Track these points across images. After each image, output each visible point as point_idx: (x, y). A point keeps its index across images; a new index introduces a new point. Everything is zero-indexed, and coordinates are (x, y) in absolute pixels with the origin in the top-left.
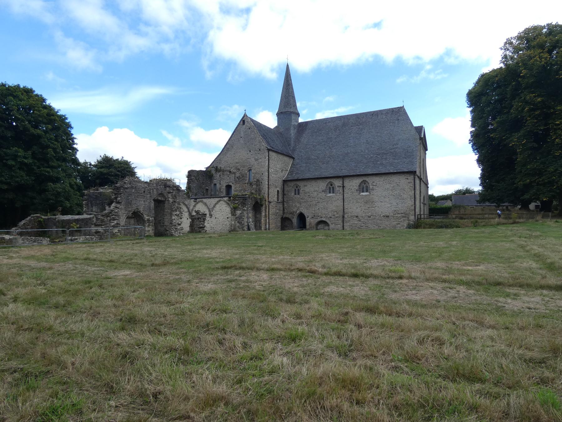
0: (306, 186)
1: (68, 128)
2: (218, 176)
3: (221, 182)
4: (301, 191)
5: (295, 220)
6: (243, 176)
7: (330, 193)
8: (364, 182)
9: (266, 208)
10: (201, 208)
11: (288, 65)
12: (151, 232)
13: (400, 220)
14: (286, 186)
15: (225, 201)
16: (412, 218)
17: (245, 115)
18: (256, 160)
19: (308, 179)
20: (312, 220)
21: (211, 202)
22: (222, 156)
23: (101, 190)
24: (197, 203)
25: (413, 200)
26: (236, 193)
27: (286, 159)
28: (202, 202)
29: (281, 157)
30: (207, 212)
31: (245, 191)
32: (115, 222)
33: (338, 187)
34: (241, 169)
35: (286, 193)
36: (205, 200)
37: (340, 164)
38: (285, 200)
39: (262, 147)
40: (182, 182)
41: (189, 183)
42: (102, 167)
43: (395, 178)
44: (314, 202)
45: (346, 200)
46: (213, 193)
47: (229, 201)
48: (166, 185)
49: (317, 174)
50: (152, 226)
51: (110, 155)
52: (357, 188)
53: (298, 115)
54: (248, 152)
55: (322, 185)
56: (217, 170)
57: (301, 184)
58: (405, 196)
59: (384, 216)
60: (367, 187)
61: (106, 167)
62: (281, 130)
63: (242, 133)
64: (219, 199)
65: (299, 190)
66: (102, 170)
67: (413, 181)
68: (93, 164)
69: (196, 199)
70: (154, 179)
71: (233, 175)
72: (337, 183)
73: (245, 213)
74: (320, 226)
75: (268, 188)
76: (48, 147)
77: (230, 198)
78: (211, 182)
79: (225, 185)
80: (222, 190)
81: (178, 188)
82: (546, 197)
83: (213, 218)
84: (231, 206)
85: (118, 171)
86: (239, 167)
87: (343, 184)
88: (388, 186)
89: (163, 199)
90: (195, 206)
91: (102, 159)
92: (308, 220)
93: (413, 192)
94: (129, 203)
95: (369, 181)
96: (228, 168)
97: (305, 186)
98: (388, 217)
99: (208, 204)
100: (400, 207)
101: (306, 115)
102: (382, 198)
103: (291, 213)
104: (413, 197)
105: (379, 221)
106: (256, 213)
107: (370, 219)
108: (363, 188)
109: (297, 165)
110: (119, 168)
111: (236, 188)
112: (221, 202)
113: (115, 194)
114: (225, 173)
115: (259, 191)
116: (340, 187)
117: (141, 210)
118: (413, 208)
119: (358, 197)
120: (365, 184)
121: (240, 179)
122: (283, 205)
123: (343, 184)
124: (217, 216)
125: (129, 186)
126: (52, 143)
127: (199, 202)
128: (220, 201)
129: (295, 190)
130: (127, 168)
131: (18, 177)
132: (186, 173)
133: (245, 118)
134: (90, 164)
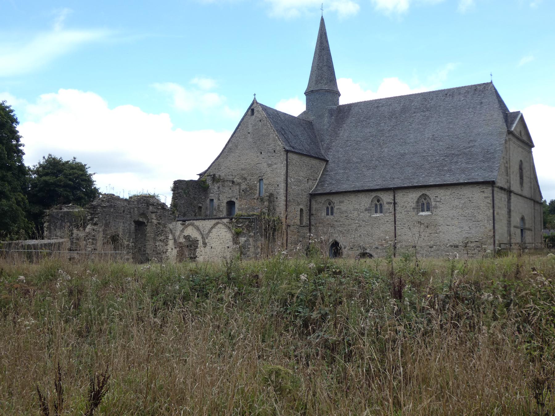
0: (342, 202)
1: (13, 123)
2: (216, 188)
3: (220, 197)
4: (335, 210)
6: (251, 189)
7: (376, 212)
8: (424, 196)
10: (190, 231)
11: (322, 20)
13: (473, 252)
14: (313, 202)
15: (225, 224)
17: (255, 102)
19: (346, 192)
21: (206, 224)
22: (221, 160)
23: (66, 210)
24: (186, 227)
25: (491, 222)
26: (240, 213)
27: (314, 162)
28: (192, 225)
29: (307, 160)
30: (199, 238)
31: (253, 209)
33: (389, 203)
34: (248, 178)
35: (313, 212)
36: (197, 223)
37: (391, 171)
38: (313, 223)
39: (278, 148)
40: (167, 199)
41: (174, 198)
42: (47, 174)
43: (467, 192)
44: (354, 226)
46: (208, 213)
47: (230, 223)
48: (147, 203)
49: (358, 185)
51: (57, 155)
52: (414, 205)
53: (339, 94)
55: (366, 201)
56: (215, 179)
57: (335, 199)
58: (480, 217)
59: (451, 246)
60: (428, 204)
61: (53, 174)
62: (311, 118)
64: (217, 221)
65: (332, 208)
66: (47, 178)
67: (491, 195)
68: (32, 168)
69: (184, 221)
70: (135, 196)
71: (238, 187)
72: (386, 198)
73: (251, 240)
75: (286, 205)
77: (231, 219)
78: (206, 197)
79: (225, 201)
80: (221, 209)
81: (163, 205)
83: (208, 247)
84: (233, 231)
85: (70, 180)
86: (246, 175)
87: (394, 200)
88: (456, 203)
90: (182, 231)
91: (47, 161)
93: (491, 211)
95: (430, 196)
96: (230, 178)
97: (340, 202)
98: (457, 247)
100: (473, 232)
101: (352, 90)
102: (449, 219)
104: (492, 218)
107: (432, 249)
108: (424, 204)
109: (331, 171)
110: (70, 174)
111: (241, 205)
112: (219, 225)
113: (92, 214)
114: (226, 183)
115: (271, 209)
116: (391, 203)
118: (491, 234)
120: (425, 199)
121: (247, 192)
123: (394, 200)
124: (213, 245)
125: (107, 204)
127: (189, 225)
128: (217, 223)
129: (328, 208)
130: (82, 175)
132: (172, 185)
133: (255, 105)
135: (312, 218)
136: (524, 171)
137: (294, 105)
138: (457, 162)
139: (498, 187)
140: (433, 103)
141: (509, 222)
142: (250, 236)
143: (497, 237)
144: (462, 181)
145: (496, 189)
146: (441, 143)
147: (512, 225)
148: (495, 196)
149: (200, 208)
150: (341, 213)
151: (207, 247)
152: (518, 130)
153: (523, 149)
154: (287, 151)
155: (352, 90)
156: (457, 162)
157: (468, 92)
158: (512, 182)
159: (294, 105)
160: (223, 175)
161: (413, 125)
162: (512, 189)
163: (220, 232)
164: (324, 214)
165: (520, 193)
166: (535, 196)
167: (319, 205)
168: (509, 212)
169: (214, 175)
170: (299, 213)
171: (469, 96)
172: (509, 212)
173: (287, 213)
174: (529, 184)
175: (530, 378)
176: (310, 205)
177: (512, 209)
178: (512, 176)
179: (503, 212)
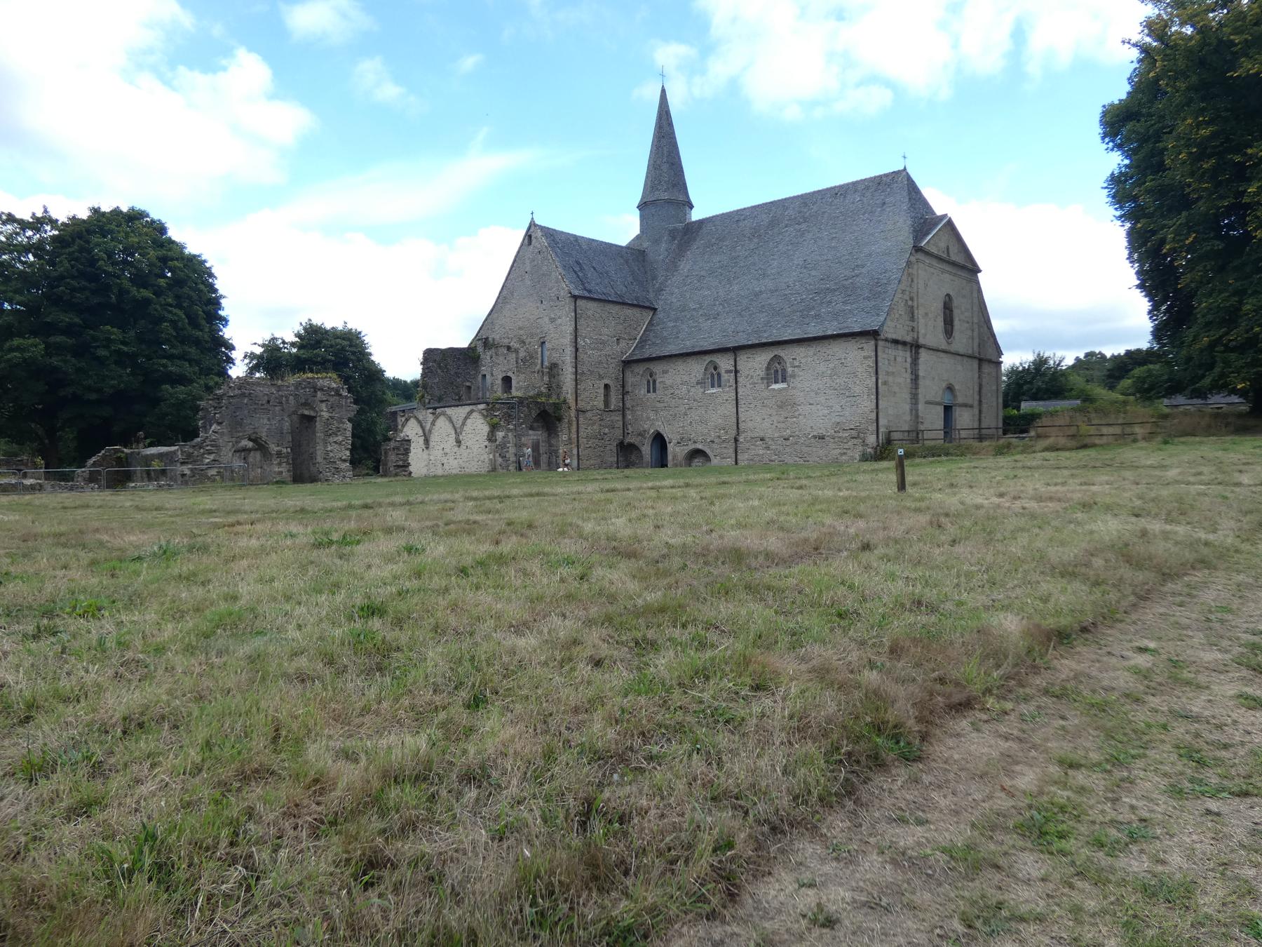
3: (493, 370)
5: (646, 449)
6: (531, 357)
7: (713, 386)
8: (777, 358)
9: (570, 423)
11: (663, 91)
12: (286, 476)
16: (872, 439)
17: (532, 224)
19: (670, 356)
20: (677, 449)
25: (874, 397)
29: (615, 309)
32: (212, 457)
33: (728, 372)
36: (449, 411)
38: (628, 405)
43: (837, 349)
44: (682, 409)
45: (741, 402)
49: (688, 346)
50: (288, 463)
51: (317, 321)
52: (762, 374)
53: (691, 207)
55: (696, 369)
57: (657, 368)
58: (857, 390)
59: (815, 437)
60: (784, 370)
62: (646, 245)
63: (528, 262)
65: (654, 381)
69: (435, 409)
72: (725, 363)
74: (697, 462)
76: (162, 319)
78: (478, 372)
79: (500, 377)
82: (1243, 380)
83: (463, 447)
88: (822, 368)
89: (312, 414)
92: (671, 448)
93: (874, 379)
94: (236, 424)
96: (506, 341)
97: (665, 372)
100: (847, 414)
101: (709, 197)
102: (813, 394)
103: (640, 434)
105: (805, 449)
106: (549, 435)
107: (788, 443)
108: (776, 373)
112: (474, 414)
116: (730, 371)
117: (264, 434)
118: (873, 416)
119: (766, 394)
122: (624, 416)
125: (237, 392)
126: (170, 312)
128: (472, 412)
131: (113, 379)
134: (284, 342)
135: (627, 397)
136: (956, 312)
137: (620, 225)
138: (830, 302)
139: (886, 340)
140: (815, 208)
141: (914, 397)
142: (509, 430)
143: (882, 422)
144: (829, 333)
145: (881, 343)
146: (813, 273)
147: (921, 398)
148: (880, 354)
149: (469, 388)
150: (666, 388)
152: (943, 245)
153: (955, 275)
154: (575, 298)
155: (709, 197)
156: (830, 302)
157: (867, 188)
158: (922, 331)
159: (620, 225)
160: (497, 337)
161: (780, 247)
162: (921, 341)
164: (643, 391)
165: (944, 346)
166: (986, 350)
167: (635, 378)
168: (915, 379)
169: (487, 339)
170: (602, 391)
171: (868, 194)
172: (915, 379)
173: (584, 394)
174: (969, 333)
175: (533, 706)
177: (921, 373)
178: (922, 321)
179: (901, 380)
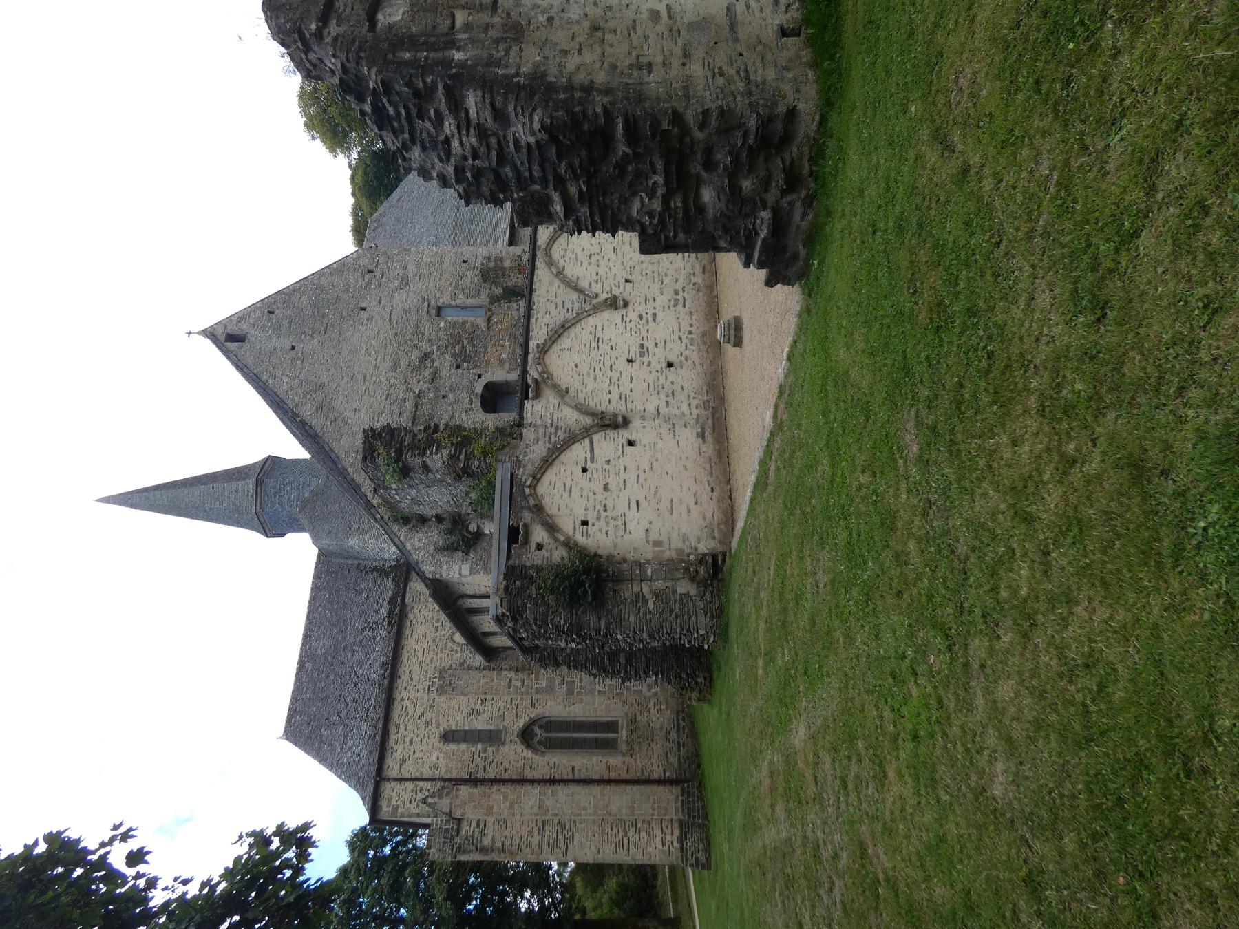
18: (405, 283)
28: (544, 350)
34: (425, 346)
54: (364, 315)
86: (416, 355)
99: (557, 317)
111: (501, 363)
128: (550, 263)
151: (626, 295)
163: (578, 251)
176: (532, 781)
